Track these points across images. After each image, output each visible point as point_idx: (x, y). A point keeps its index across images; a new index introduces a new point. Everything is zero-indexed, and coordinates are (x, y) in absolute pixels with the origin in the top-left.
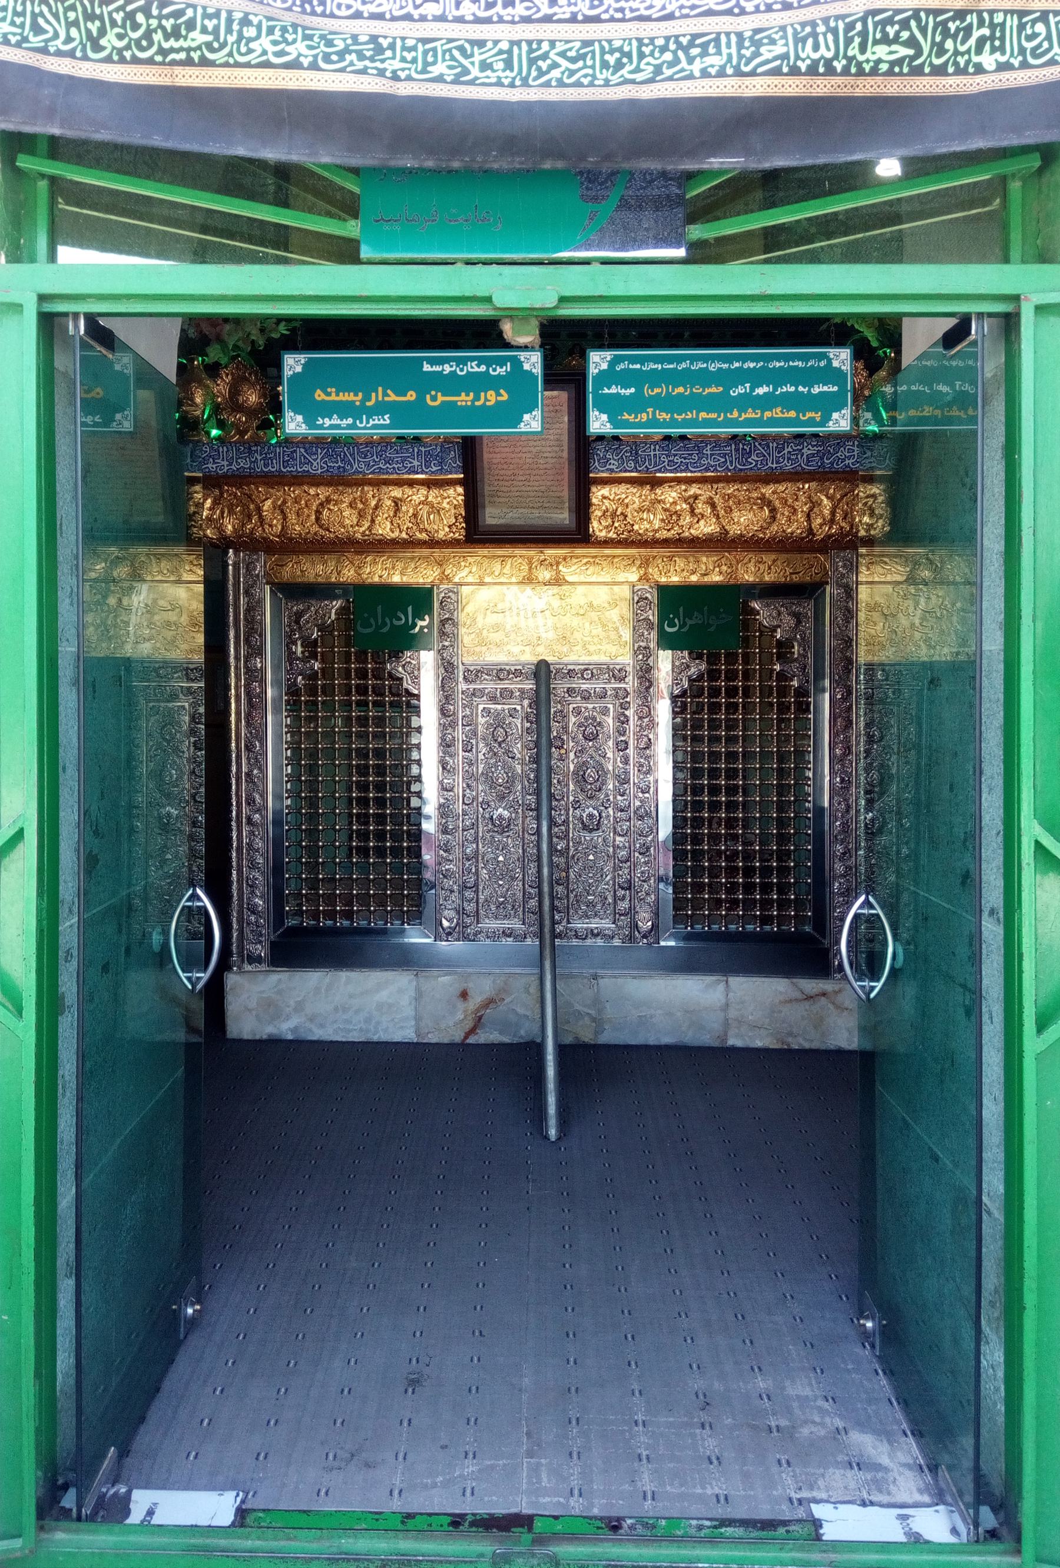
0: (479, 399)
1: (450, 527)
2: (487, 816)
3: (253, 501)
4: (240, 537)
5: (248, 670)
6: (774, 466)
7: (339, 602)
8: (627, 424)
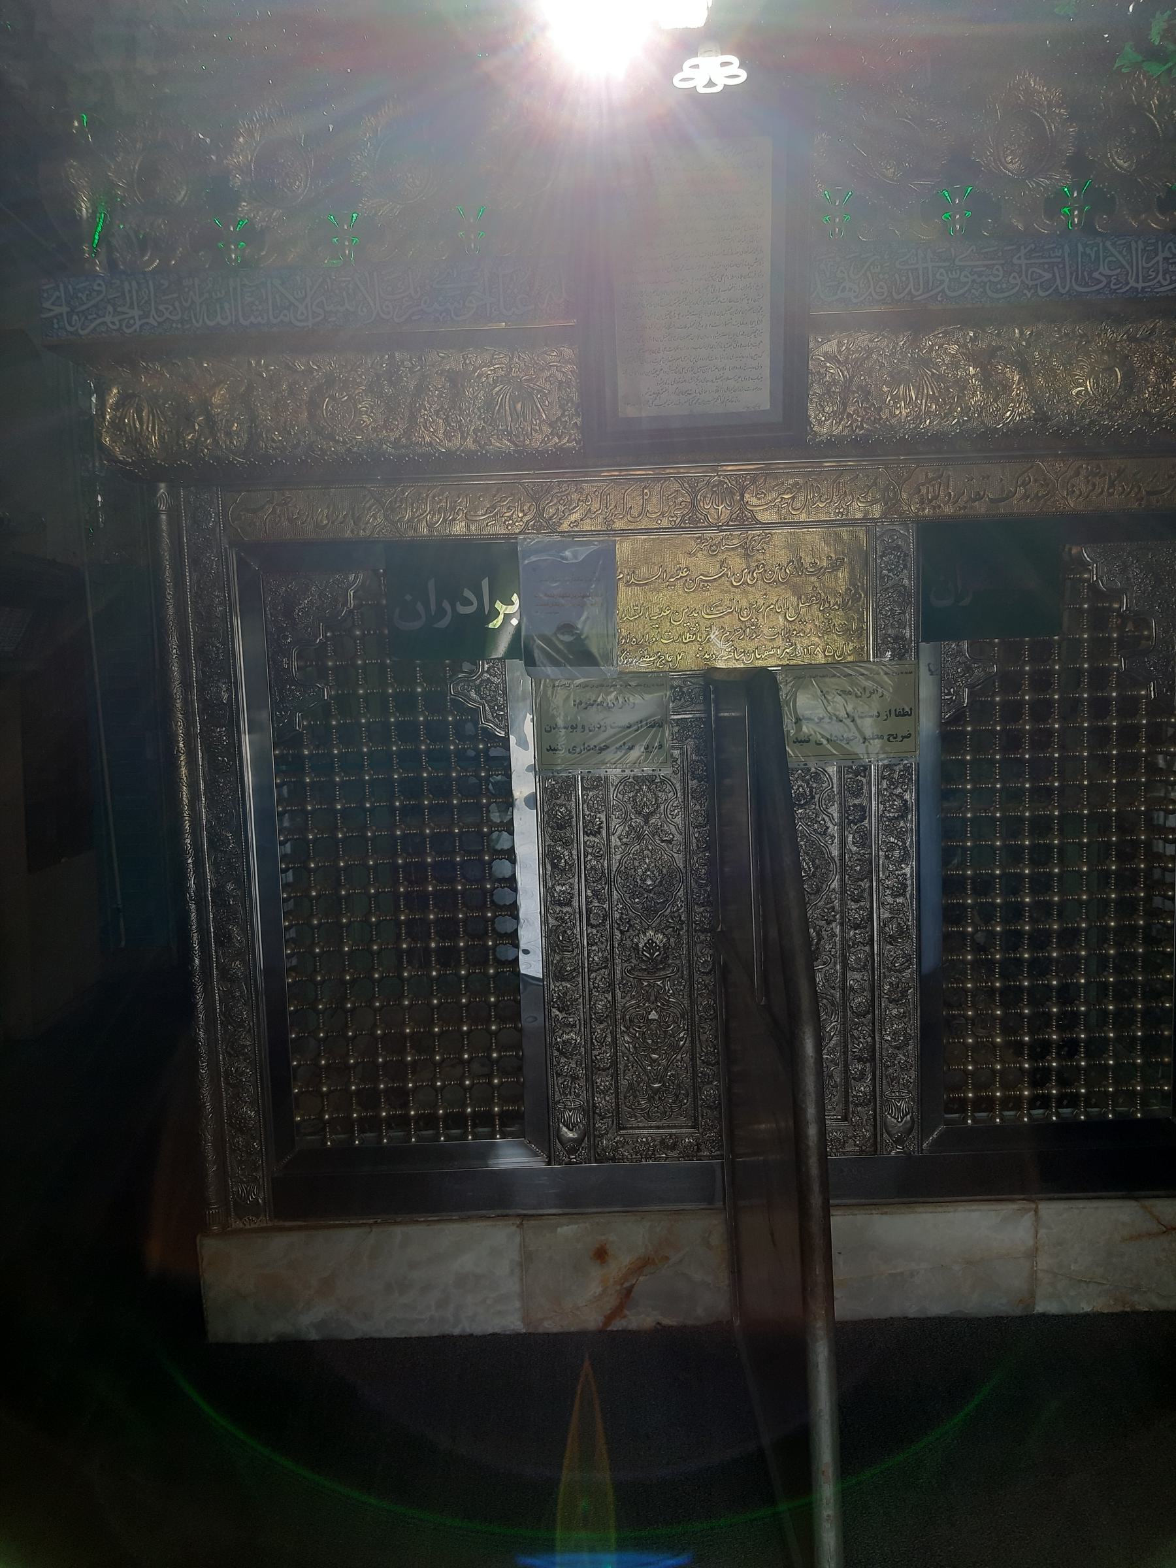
2: (628, 943)
5: (206, 706)
6: (1140, 285)
7: (361, 576)
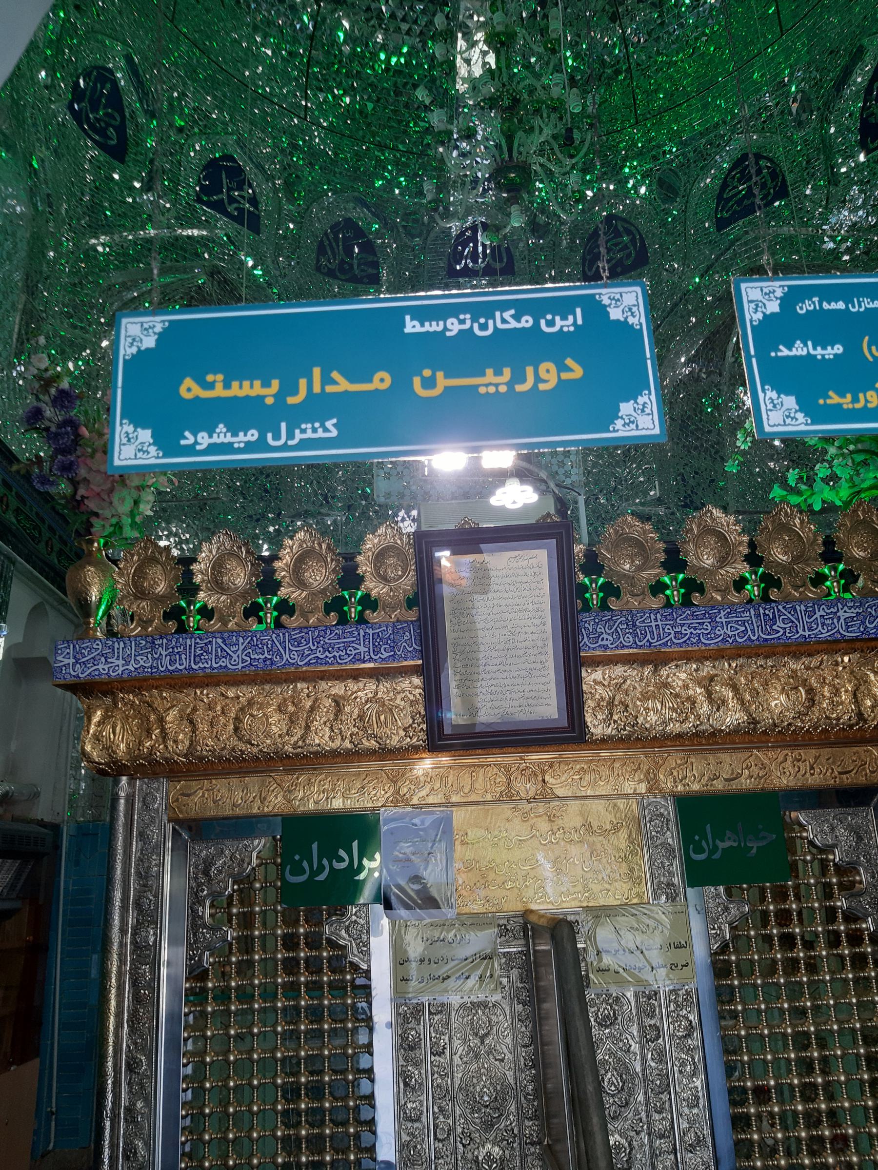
0: (524, 380)
1: (405, 730)
2: (470, 1156)
3: (154, 710)
4: (139, 757)
8: (837, 414)
